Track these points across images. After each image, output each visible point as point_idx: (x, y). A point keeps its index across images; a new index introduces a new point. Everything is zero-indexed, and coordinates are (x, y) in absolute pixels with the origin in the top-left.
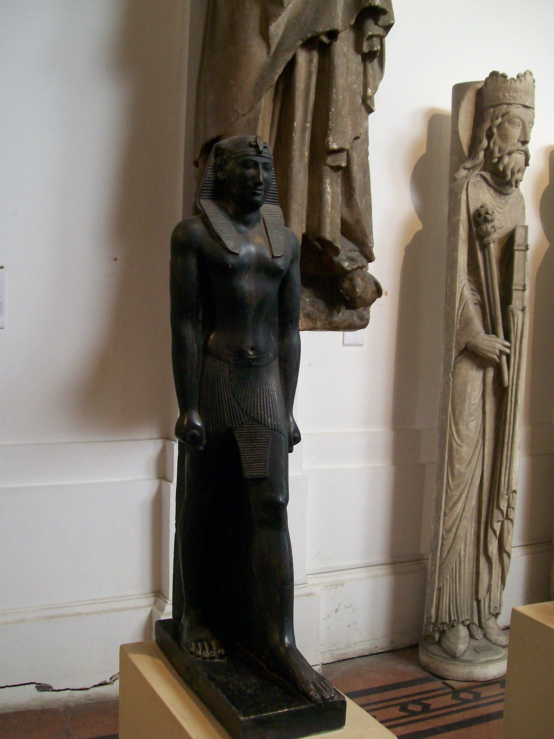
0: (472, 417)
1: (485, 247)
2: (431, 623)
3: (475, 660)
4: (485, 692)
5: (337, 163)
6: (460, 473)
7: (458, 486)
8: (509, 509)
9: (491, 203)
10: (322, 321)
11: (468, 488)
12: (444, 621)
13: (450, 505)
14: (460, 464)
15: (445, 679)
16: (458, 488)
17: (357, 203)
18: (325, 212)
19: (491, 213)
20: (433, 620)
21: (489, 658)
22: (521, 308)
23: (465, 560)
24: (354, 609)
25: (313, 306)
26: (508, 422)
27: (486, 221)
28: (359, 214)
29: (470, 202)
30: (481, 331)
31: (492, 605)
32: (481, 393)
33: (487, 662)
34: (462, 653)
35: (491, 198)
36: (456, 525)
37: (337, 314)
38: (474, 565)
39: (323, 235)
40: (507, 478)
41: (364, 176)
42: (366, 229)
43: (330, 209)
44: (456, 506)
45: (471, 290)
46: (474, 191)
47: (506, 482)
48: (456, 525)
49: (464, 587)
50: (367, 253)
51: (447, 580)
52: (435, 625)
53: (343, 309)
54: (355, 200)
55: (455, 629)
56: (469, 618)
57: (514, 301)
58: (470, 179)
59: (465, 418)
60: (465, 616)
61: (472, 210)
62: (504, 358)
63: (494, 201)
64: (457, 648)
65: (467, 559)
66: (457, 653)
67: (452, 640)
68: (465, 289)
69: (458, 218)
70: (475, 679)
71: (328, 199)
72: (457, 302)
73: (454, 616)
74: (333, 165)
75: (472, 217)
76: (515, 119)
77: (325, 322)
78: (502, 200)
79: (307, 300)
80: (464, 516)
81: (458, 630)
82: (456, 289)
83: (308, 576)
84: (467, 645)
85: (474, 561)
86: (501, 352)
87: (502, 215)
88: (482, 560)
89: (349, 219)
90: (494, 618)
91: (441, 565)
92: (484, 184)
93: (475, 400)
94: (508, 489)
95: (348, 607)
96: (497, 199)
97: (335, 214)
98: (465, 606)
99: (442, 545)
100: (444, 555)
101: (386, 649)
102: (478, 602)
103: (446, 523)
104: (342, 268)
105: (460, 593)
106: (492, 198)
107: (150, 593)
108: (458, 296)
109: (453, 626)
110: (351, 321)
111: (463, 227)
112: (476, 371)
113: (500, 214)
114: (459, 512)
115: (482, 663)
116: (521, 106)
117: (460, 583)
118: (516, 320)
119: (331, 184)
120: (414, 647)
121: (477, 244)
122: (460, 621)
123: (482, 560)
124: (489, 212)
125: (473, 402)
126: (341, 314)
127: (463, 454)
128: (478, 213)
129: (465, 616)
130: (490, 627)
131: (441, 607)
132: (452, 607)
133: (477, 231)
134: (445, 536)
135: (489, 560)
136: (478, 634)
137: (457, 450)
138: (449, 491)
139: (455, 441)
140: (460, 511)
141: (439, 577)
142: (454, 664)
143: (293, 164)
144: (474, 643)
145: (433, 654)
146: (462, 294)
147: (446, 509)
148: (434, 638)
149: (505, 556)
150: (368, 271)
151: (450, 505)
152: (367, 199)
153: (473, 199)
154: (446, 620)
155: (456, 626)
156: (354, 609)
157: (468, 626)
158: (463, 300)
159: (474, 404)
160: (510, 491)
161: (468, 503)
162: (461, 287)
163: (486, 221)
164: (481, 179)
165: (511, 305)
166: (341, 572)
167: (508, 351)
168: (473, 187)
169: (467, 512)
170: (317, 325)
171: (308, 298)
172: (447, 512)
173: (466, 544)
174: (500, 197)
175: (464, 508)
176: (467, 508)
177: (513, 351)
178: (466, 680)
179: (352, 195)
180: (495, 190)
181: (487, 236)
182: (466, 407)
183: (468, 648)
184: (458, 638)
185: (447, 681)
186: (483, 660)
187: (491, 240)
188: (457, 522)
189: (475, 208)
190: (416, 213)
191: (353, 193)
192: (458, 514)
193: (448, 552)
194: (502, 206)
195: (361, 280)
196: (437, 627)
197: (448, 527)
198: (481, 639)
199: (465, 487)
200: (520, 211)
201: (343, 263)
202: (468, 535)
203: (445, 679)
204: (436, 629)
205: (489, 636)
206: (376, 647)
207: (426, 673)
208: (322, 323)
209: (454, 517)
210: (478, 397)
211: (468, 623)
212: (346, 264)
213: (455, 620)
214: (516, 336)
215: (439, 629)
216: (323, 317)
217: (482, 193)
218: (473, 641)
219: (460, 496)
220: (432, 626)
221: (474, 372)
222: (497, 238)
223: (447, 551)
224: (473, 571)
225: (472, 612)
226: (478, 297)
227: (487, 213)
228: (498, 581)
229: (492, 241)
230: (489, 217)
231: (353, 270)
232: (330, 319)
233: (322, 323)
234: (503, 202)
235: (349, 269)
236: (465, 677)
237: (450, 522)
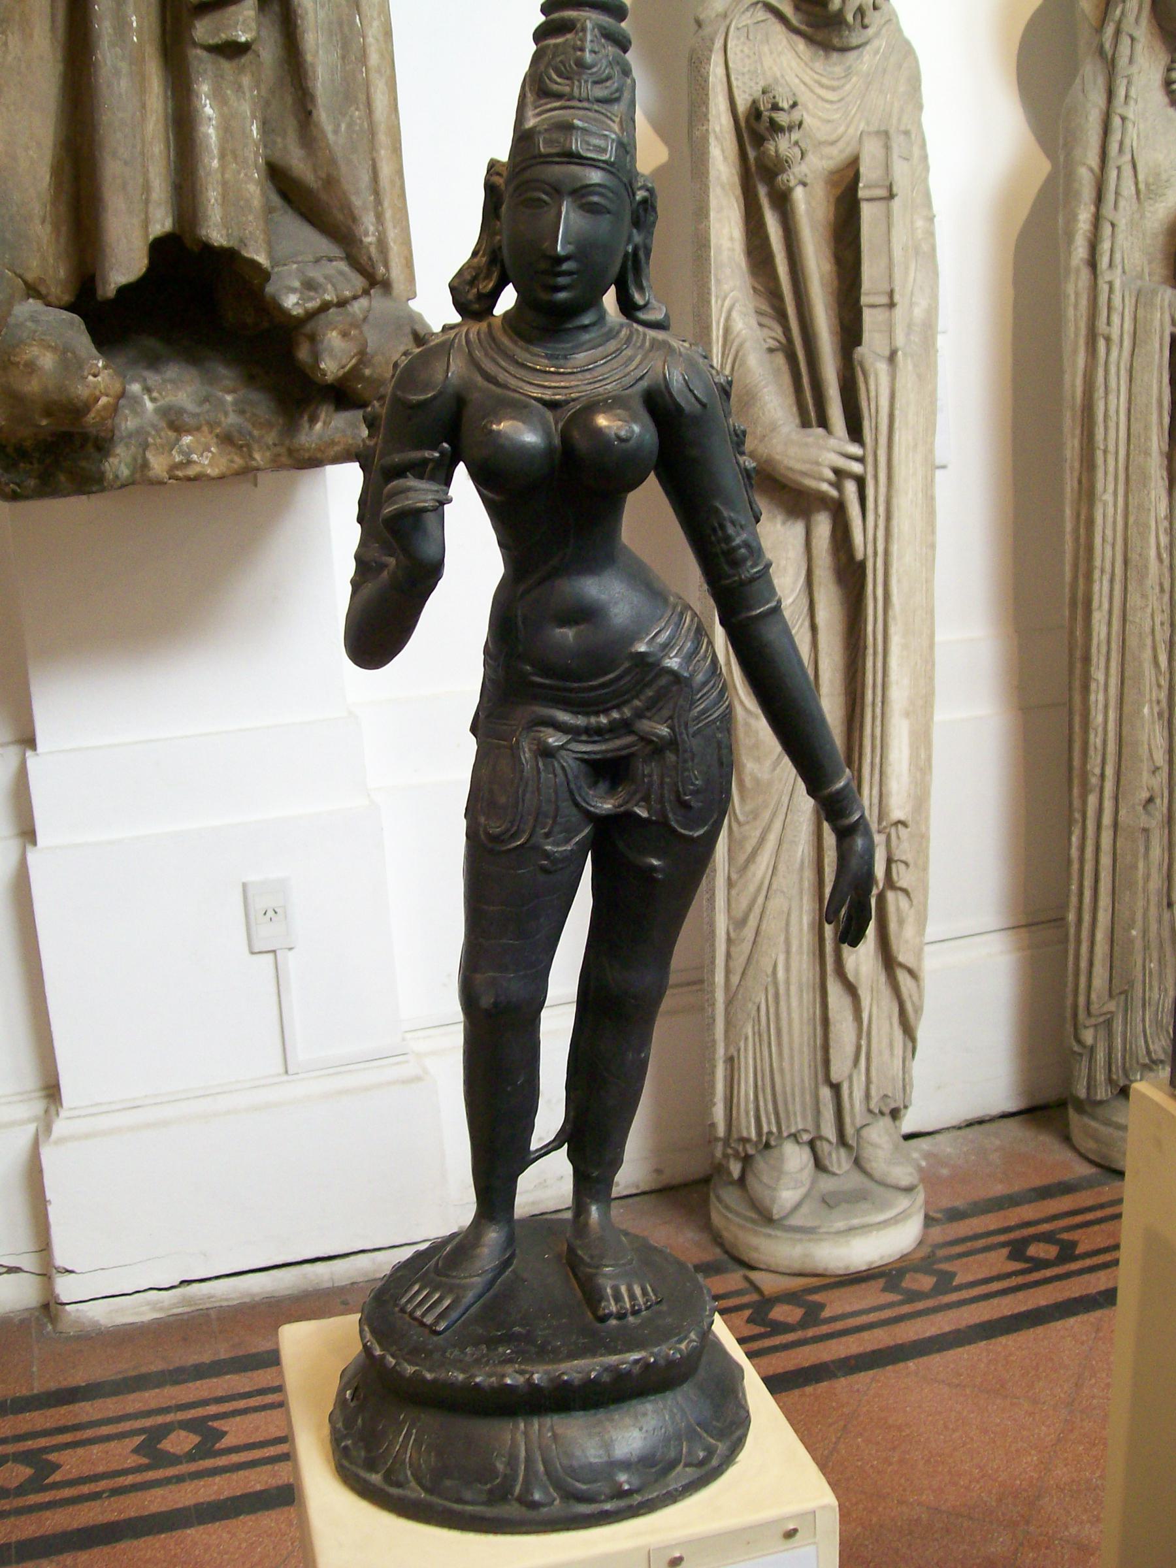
1: (782, 201)
2: (717, 1139)
3: (819, 1227)
4: (837, 1304)
5: (223, 36)
6: (757, 781)
7: (755, 815)
8: (894, 866)
9: (797, 76)
10: (268, 448)
11: (781, 817)
12: (745, 1134)
13: (741, 858)
14: (758, 760)
15: (752, 1268)
16: (755, 818)
17: (323, 132)
18: (202, 173)
19: (786, 106)
20: (721, 1131)
21: (856, 1222)
22: (887, 353)
23: (788, 990)
25: (242, 412)
26: (870, 651)
27: (776, 128)
28: (333, 162)
29: (734, 83)
30: (781, 422)
31: (873, 1092)
32: (802, 580)
33: (851, 1230)
34: (786, 1211)
36: (757, 910)
37: (306, 426)
38: (815, 1001)
39: (203, 232)
40: (875, 791)
41: (343, 58)
42: (353, 198)
43: (216, 161)
44: (754, 862)
45: (756, 312)
46: (746, 50)
47: (876, 800)
48: (757, 910)
49: (792, 1058)
50: (362, 261)
51: (746, 1039)
52: (727, 1141)
53: (324, 412)
54: (317, 125)
55: (775, 1153)
56: (810, 1126)
57: (866, 336)
58: (731, 21)
60: (799, 1122)
61: (742, 106)
62: (851, 488)
64: (773, 1200)
65: (794, 989)
66: (775, 1211)
67: (765, 1179)
68: (735, 314)
69: (705, 128)
70: (820, 1271)
71: (207, 136)
72: (715, 350)
73: (769, 1123)
74: (211, 42)
75: (743, 124)
77: (279, 449)
78: (836, 65)
79: (229, 398)
80: (774, 887)
81: (782, 1155)
82: (710, 316)
83: (408, 1036)
84: (802, 1191)
85: (814, 992)
86: (838, 472)
87: (835, 107)
88: (834, 989)
89: (625, 140)
90: (887, 1120)
91: (729, 1003)
92: (777, 28)
94: (880, 821)
96: (818, 65)
97: (239, 172)
98: (797, 1099)
99: (728, 955)
100: (735, 980)
101: (644, 1187)
102: (836, 1088)
103: (733, 906)
104: (284, 312)
105: (782, 1070)
107: (34, 1091)
108: (717, 334)
109: (767, 1146)
110: (350, 441)
111: (723, 151)
112: (784, 523)
113: (828, 106)
114: (764, 878)
115: (839, 1233)
117: (779, 1044)
118: (872, 387)
119: (218, 96)
120: (704, 1183)
121: (762, 191)
122: (785, 1134)
123: (834, 989)
124: (780, 105)
126: (319, 426)
128: (755, 113)
129: (799, 1122)
130: (872, 1145)
131: (735, 1100)
132: (761, 1104)
133: (757, 159)
134: (733, 935)
135: (851, 990)
136: (839, 1161)
137: (747, 724)
138: (735, 826)
139: (742, 703)
141: (726, 1032)
142: (770, 1236)
143: (99, 56)
144: (827, 1184)
145: (727, 1207)
146: (727, 331)
147: (732, 869)
148: (729, 1173)
149: (902, 977)
150: (411, 303)
151: (741, 858)
152: (351, 117)
153: (743, 74)
154: (749, 1133)
155: (776, 1146)
157: (812, 1144)
158: (732, 343)
160: (884, 824)
161: (784, 856)
162: (725, 309)
163: (776, 128)
164: (769, 16)
165: (859, 348)
167: (856, 468)
168: (743, 39)
169: (784, 877)
170: (254, 459)
171: (229, 392)
172: (734, 876)
173: (788, 952)
174: (827, 57)
175: (775, 868)
176: (782, 868)
177: (870, 468)
178: (796, 1271)
179: (310, 113)
180: (810, 40)
181: (783, 171)
183: (806, 1196)
184: (778, 1171)
185: (755, 1276)
186: (841, 1225)
187: (792, 177)
188: (760, 900)
189: (751, 95)
190: (646, 122)
191: (310, 107)
192: (762, 883)
193: (743, 973)
194: (835, 83)
195: (339, 337)
196: (731, 1148)
197: (738, 913)
198: (847, 1172)
199: (774, 815)
200: (902, 89)
201: (283, 297)
202: (794, 930)
203: (752, 1268)
204: (730, 1151)
205: (868, 1166)
207: (718, 1251)
208: (268, 454)
209: (752, 888)
210: (793, 590)
211: (806, 1137)
212: (291, 302)
213: (770, 1133)
214: (876, 428)
215: (737, 1152)
216: (271, 437)
217: (771, 53)
218: (823, 1177)
219: (762, 840)
220: (720, 1146)
221: (779, 526)
222: (823, 169)
223: (739, 971)
224: (814, 1013)
225: (818, 1113)
226: (779, 332)
227: (775, 107)
228: (891, 1035)
229: (797, 181)
230: (782, 118)
231: (311, 315)
232: (287, 442)
233: (268, 454)
234: (838, 70)
235: (297, 311)
236: (797, 1266)
237: (744, 904)
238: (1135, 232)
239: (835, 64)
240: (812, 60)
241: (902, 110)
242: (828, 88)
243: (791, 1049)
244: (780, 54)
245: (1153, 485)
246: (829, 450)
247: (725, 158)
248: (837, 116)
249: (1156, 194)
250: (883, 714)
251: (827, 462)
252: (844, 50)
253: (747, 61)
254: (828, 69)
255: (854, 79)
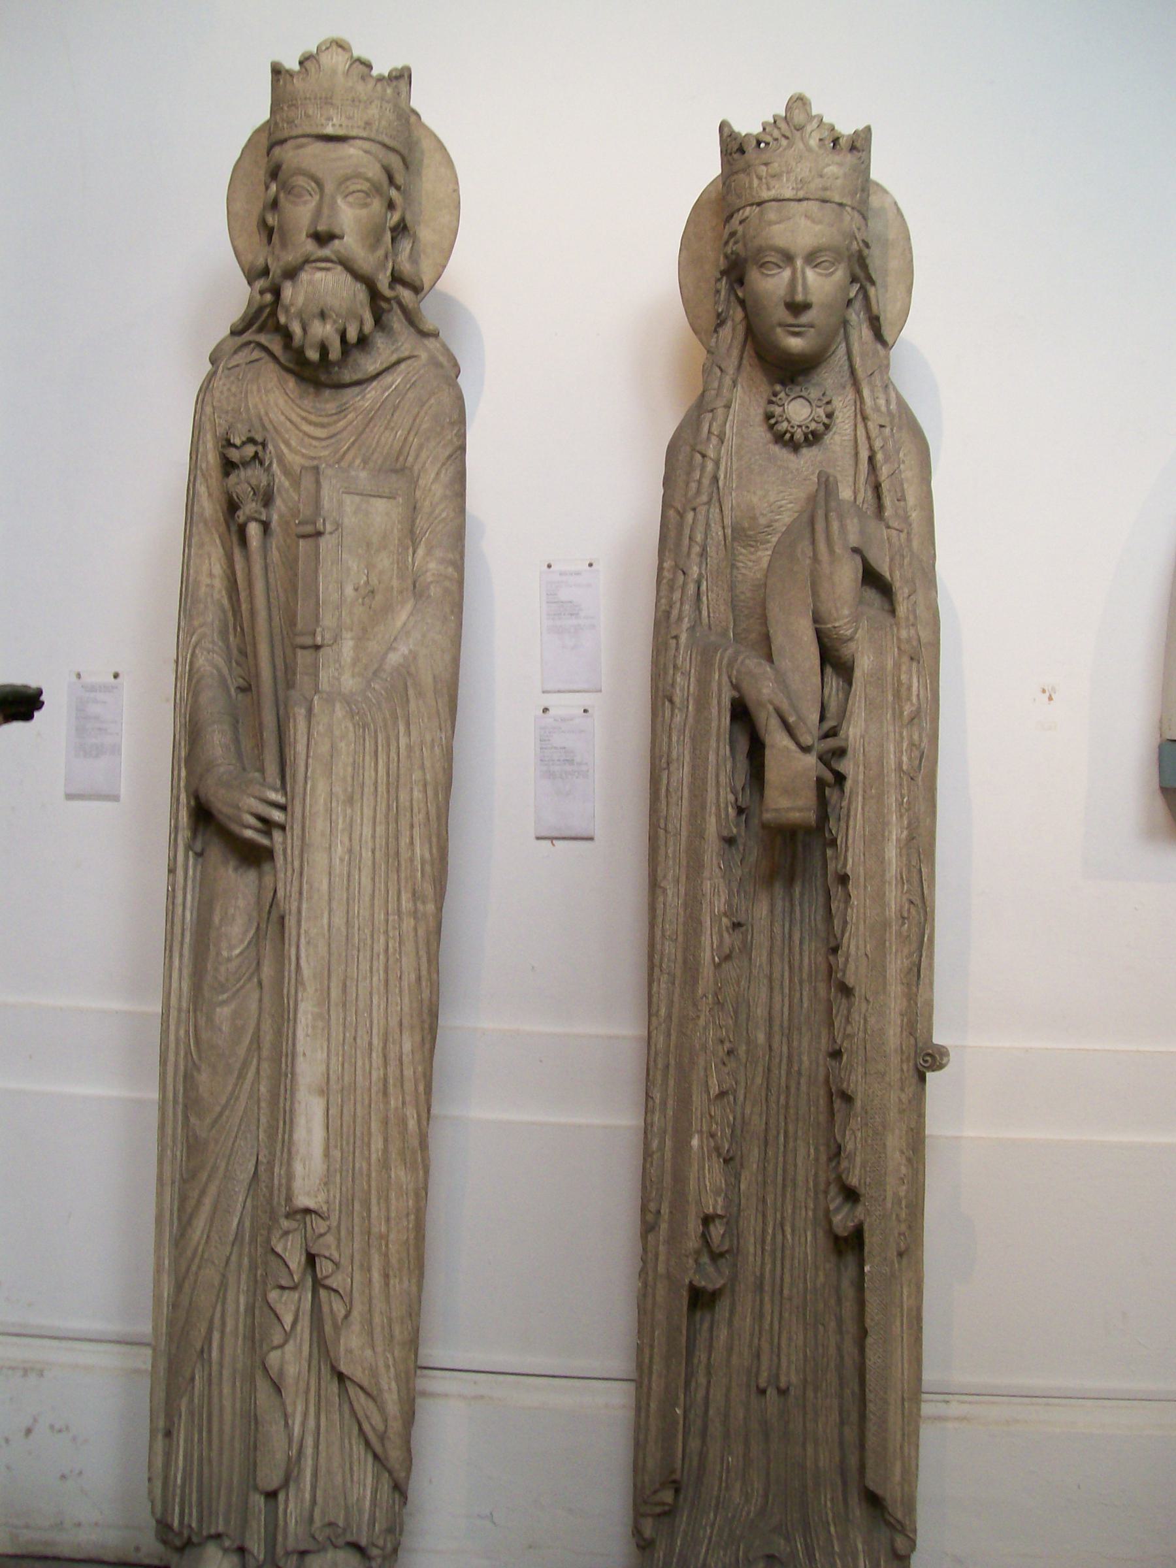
0: (223, 993)
9: (283, 413)
24: (74, 1439)
35: (286, 401)
46: (234, 389)
49: (221, 1449)
59: (207, 994)
63: (295, 408)
65: (226, 1373)
76: (294, 178)
87: (324, 443)
92: (272, 366)
93: (231, 948)
95: (60, 1431)
96: (307, 403)
106: (290, 402)
112: (236, 869)
113: (314, 443)
116: (309, 140)
125: (225, 954)
127: (201, 1089)
140: (201, 1238)
153: (227, 412)
156: (74, 1439)
159: (229, 960)
164: (263, 354)
166: (55, 1343)
182: (209, 967)
194: (326, 420)
206: (137, 1549)
210: (242, 941)
221: (230, 871)
234: (331, 407)
238: (720, 583)
239: (327, 401)
240: (301, 397)
241: (421, 447)
242: (315, 425)
243: (221, 1441)
244: (267, 392)
245: (706, 874)
246: (250, 795)
247: (210, 495)
248: (325, 453)
249: (756, 541)
250: (291, 1089)
251: (246, 807)
252: (340, 386)
253: (232, 399)
254: (318, 405)
255: (351, 416)
